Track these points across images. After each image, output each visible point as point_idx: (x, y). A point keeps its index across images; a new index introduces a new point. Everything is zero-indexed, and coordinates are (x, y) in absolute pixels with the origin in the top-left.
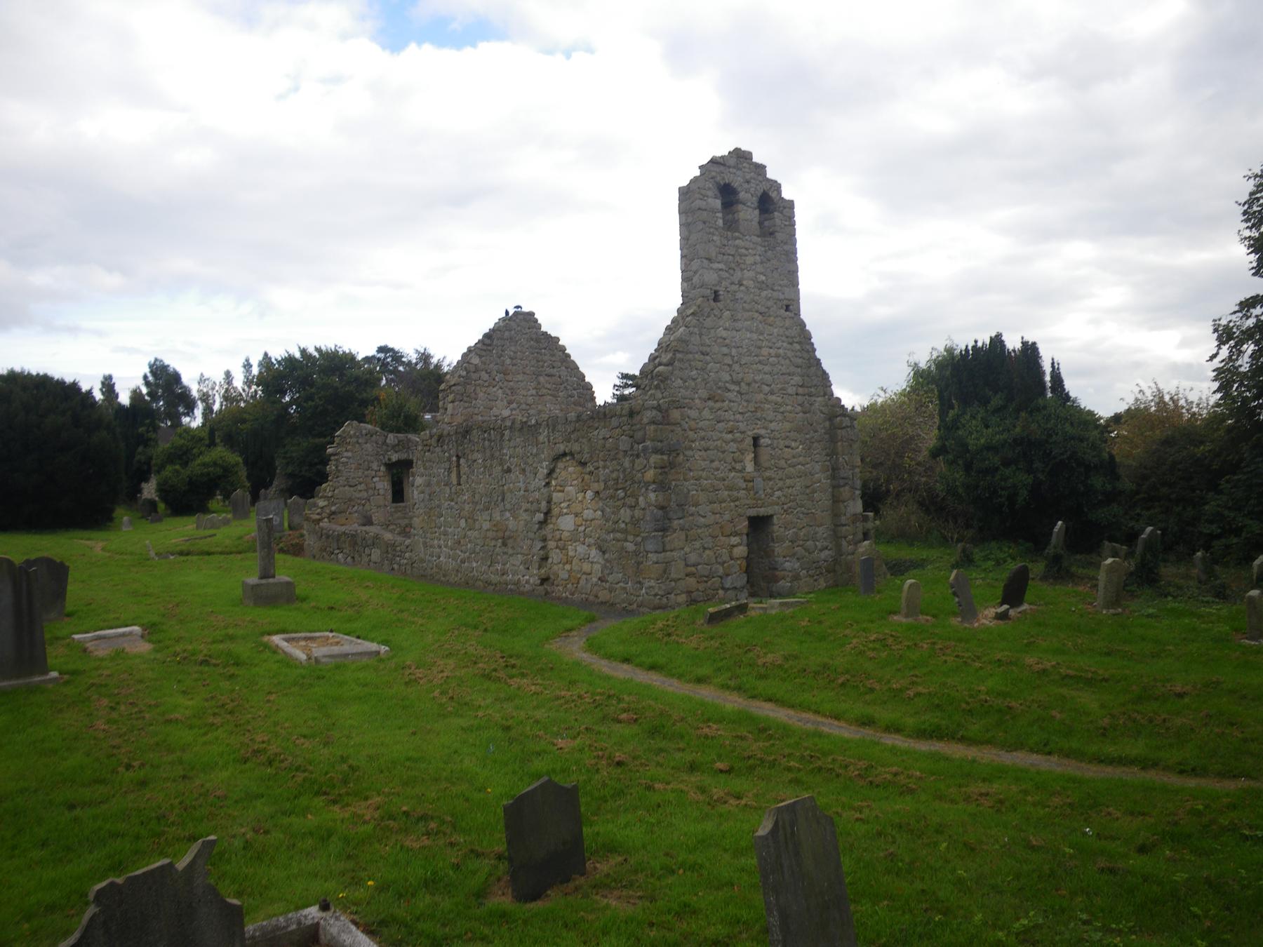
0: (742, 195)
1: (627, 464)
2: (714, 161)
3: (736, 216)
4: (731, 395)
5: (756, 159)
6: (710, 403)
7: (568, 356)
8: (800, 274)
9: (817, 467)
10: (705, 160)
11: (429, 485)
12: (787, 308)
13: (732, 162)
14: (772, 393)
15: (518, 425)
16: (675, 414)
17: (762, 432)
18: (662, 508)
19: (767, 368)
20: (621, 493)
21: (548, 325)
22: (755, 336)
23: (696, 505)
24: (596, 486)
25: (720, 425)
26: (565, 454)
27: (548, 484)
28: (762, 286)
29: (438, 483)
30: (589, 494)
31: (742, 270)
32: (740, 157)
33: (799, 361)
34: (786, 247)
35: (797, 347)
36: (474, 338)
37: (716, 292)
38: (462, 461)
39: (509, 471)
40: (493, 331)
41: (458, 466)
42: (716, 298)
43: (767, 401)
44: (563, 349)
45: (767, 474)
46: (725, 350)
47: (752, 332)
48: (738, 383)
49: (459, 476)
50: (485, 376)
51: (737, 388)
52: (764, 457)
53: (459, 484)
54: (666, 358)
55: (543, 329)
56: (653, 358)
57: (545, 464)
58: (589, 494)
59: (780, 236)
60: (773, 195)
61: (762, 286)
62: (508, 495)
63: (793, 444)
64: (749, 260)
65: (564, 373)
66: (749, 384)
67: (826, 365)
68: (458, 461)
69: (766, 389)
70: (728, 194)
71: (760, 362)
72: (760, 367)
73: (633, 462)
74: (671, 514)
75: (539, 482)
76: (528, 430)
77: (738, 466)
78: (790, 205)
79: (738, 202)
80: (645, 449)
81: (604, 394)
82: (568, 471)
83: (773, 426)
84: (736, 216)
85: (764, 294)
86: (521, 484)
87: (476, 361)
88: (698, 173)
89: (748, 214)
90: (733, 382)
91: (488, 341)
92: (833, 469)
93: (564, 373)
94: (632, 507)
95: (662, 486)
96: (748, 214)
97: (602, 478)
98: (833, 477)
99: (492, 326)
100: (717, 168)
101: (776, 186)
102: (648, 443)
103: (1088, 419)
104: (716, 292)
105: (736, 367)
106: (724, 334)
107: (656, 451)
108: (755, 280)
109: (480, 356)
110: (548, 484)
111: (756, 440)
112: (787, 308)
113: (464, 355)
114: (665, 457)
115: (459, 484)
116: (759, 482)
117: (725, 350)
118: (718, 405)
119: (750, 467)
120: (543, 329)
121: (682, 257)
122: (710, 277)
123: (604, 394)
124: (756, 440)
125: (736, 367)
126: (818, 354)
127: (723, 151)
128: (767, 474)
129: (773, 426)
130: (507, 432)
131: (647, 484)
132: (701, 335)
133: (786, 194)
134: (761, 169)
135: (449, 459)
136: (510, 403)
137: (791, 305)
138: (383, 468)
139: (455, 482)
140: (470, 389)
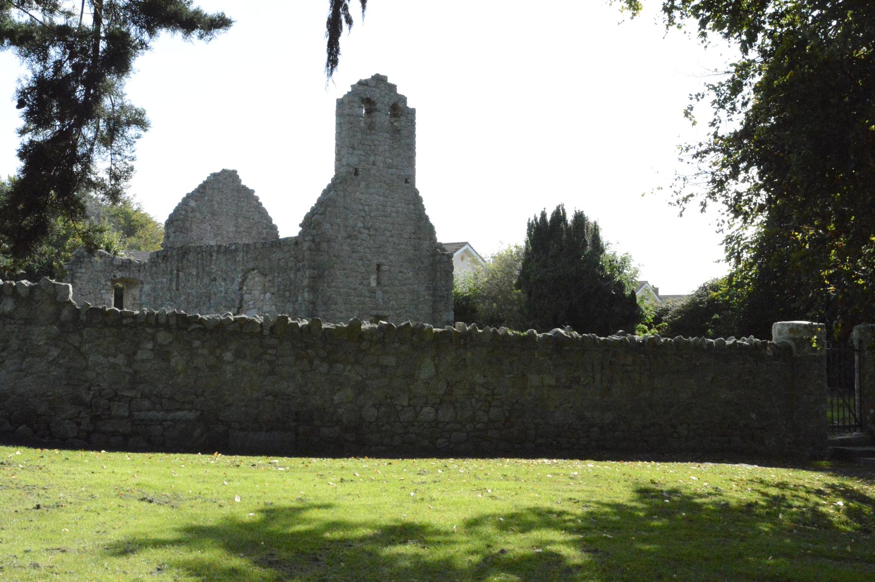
0: (378, 105)
1: (292, 276)
2: (360, 83)
3: (376, 122)
4: (364, 236)
5: (390, 81)
6: (348, 240)
7: (260, 204)
8: (417, 158)
10: (355, 82)
11: (154, 289)
13: (373, 83)
14: (392, 236)
15: (222, 250)
16: (324, 245)
17: (384, 261)
19: (389, 220)
21: (246, 181)
22: (382, 198)
23: (336, 304)
25: (355, 255)
27: (241, 289)
28: (390, 167)
29: (162, 288)
32: (379, 80)
34: (408, 141)
35: (412, 207)
36: (191, 186)
37: (356, 169)
40: (205, 183)
42: (356, 174)
43: (388, 241)
44: (257, 199)
45: (386, 288)
46: (361, 207)
47: (380, 196)
48: (369, 229)
49: (178, 284)
50: (198, 215)
51: (367, 231)
52: (384, 279)
53: (178, 289)
55: (243, 183)
56: (313, 209)
57: (240, 275)
58: (268, 295)
59: (404, 133)
60: (401, 105)
61: (390, 167)
62: (213, 297)
64: (381, 149)
65: (257, 217)
67: (432, 220)
69: (388, 234)
70: (369, 103)
72: (385, 219)
73: (296, 274)
75: (236, 287)
76: (227, 251)
78: (412, 112)
80: (304, 266)
81: (288, 226)
83: (391, 258)
84: (376, 122)
85: (390, 171)
86: (222, 289)
87: (193, 204)
88: (350, 90)
89: (383, 118)
90: (365, 228)
92: (434, 290)
94: (294, 302)
96: (383, 118)
97: (276, 284)
98: (433, 295)
99: (205, 179)
100: (361, 88)
101: (403, 99)
103: (296, 237)
104: (356, 169)
106: (360, 196)
107: (310, 267)
108: (384, 162)
109: (196, 201)
110: (241, 289)
111: (379, 266)
112: (406, 182)
113: (184, 200)
114: (316, 272)
115: (178, 289)
116: (379, 294)
117: (361, 207)
119: (374, 284)
120: (243, 183)
122: (354, 160)
123: (288, 226)
124: (379, 266)
126: (427, 212)
127: (367, 76)
128: (386, 288)
129: (391, 258)
130: (214, 254)
134: (393, 88)
135: (171, 273)
137: (409, 180)
138: (109, 283)
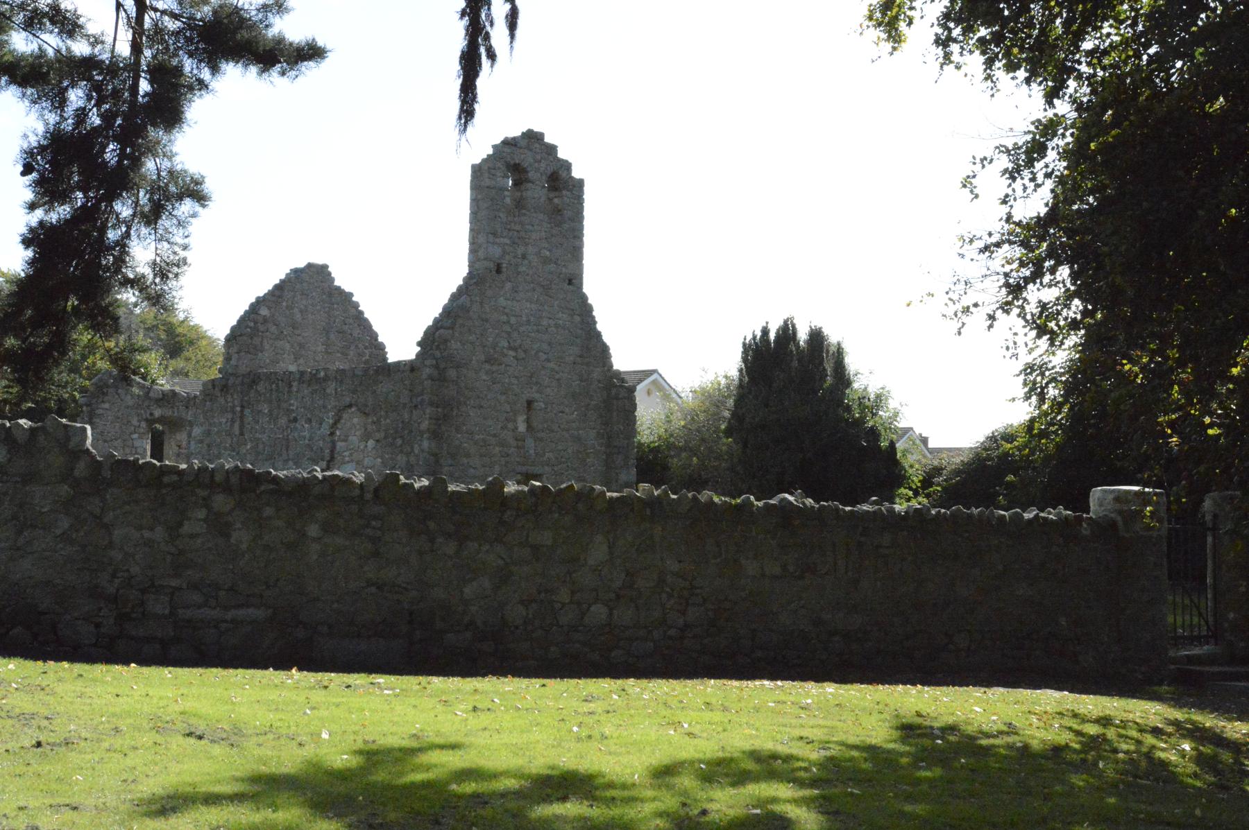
2: (506, 142)
3: (528, 198)
7: (361, 313)
9: (593, 434)
11: (208, 433)
12: (570, 282)
13: (523, 143)
14: (548, 360)
15: (307, 377)
16: (452, 373)
17: (537, 396)
18: (435, 455)
20: (399, 442)
21: (342, 280)
23: (468, 455)
24: (378, 436)
26: (350, 406)
27: (332, 434)
28: (546, 261)
30: (371, 443)
31: (527, 245)
32: (532, 138)
33: (579, 332)
35: (577, 319)
38: (247, 412)
39: (295, 420)
41: (242, 417)
44: (356, 305)
46: (504, 318)
48: (515, 349)
49: (242, 427)
50: (273, 329)
54: (448, 323)
58: (371, 443)
60: (564, 174)
63: (567, 410)
66: (525, 351)
68: (242, 411)
70: (517, 170)
71: (538, 331)
74: (442, 461)
76: (313, 380)
77: (510, 425)
78: (580, 183)
79: (528, 181)
82: (353, 420)
84: (528, 198)
86: (306, 434)
87: (264, 312)
88: (491, 152)
89: (537, 192)
90: (510, 348)
91: (277, 293)
93: (356, 333)
94: (408, 454)
95: (435, 435)
96: (537, 192)
99: (283, 277)
100: (507, 150)
101: (567, 166)
102: (426, 397)
103: (411, 362)
105: (515, 335)
110: (332, 434)
112: (570, 282)
116: (530, 443)
117: (504, 318)
118: (495, 368)
119: (522, 427)
121: (472, 230)
122: (496, 251)
123: (401, 343)
124: (530, 403)
125: (515, 335)
127: (516, 132)
130: (295, 384)
131: (422, 433)
132: (481, 303)
133: (576, 173)
134: (552, 149)
136: (296, 359)
139: (237, 433)
140: (257, 341)
